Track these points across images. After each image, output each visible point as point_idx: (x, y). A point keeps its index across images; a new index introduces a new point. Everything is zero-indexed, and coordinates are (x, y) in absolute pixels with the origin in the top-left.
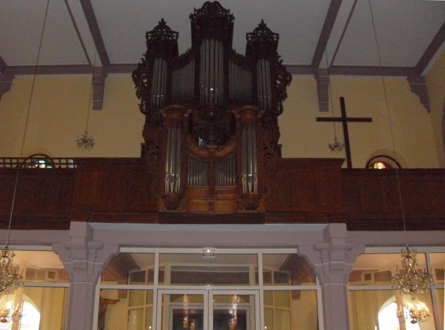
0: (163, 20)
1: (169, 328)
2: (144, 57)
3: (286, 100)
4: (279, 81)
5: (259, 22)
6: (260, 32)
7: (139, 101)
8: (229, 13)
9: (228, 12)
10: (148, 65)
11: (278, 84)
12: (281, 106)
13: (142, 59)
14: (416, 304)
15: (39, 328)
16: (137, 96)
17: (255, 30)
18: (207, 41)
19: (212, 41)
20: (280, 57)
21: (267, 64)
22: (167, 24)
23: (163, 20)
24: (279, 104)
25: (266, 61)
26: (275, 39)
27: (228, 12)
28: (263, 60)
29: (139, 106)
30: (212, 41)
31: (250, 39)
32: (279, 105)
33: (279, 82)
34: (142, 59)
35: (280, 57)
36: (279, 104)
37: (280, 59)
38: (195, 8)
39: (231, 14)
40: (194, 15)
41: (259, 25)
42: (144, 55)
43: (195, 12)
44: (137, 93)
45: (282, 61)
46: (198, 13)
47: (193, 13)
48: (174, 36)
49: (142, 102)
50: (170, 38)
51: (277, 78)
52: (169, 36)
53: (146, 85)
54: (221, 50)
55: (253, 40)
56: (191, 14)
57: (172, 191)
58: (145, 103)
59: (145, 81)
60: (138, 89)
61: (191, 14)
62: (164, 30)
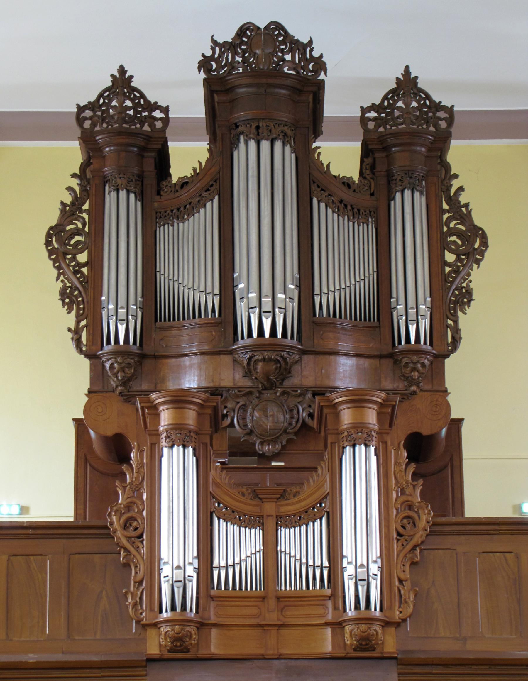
0: (122, 70)
1: (174, 198)
2: (74, 183)
3: (468, 310)
4: (451, 251)
5: (399, 73)
6: (400, 104)
7: (70, 320)
8: (312, 50)
9: (308, 49)
10: (86, 207)
11: (446, 264)
12: (456, 331)
13: (70, 189)
14: (138, 619)
15: (449, 384)
16: (64, 304)
17: (385, 98)
18: (252, 144)
19: (265, 145)
20: (456, 176)
21: (420, 200)
22: (135, 83)
23: (122, 70)
24: (450, 322)
25: (417, 195)
26: (443, 124)
27: (308, 49)
28: (407, 193)
29: (70, 335)
30: (265, 145)
31: (371, 125)
32: (448, 326)
33: (450, 257)
34: (70, 189)
35: (456, 176)
36: (450, 322)
37: (456, 184)
38: (215, 38)
39: (316, 54)
40: (212, 58)
41: (397, 83)
42: (74, 176)
43: (213, 49)
44: (63, 294)
45: (461, 189)
46: (221, 54)
47: (209, 53)
48: (155, 119)
49: (78, 322)
50: (146, 128)
51: (446, 246)
52: (142, 121)
53: (85, 270)
54: (290, 158)
55: (381, 129)
56: (203, 55)
57: (180, 611)
58: (86, 326)
59: (83, 258)
60: (62, 281)
61: (203, 55)
62: (128, 103)
